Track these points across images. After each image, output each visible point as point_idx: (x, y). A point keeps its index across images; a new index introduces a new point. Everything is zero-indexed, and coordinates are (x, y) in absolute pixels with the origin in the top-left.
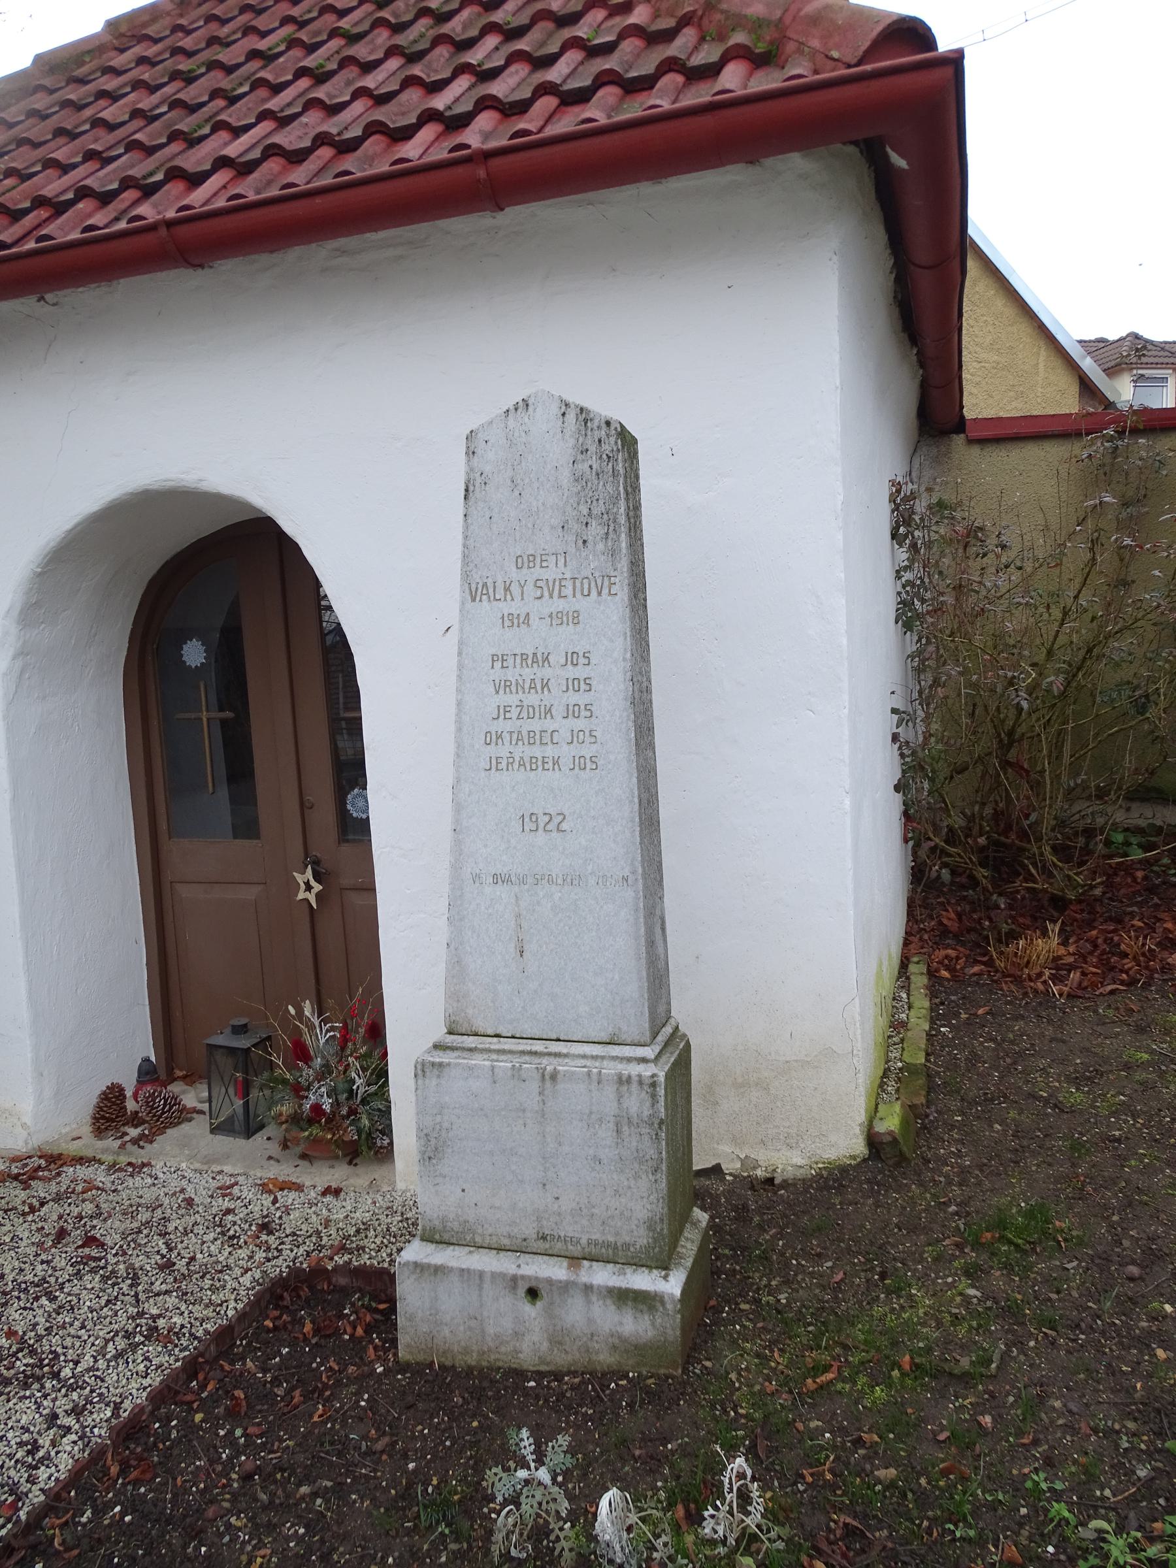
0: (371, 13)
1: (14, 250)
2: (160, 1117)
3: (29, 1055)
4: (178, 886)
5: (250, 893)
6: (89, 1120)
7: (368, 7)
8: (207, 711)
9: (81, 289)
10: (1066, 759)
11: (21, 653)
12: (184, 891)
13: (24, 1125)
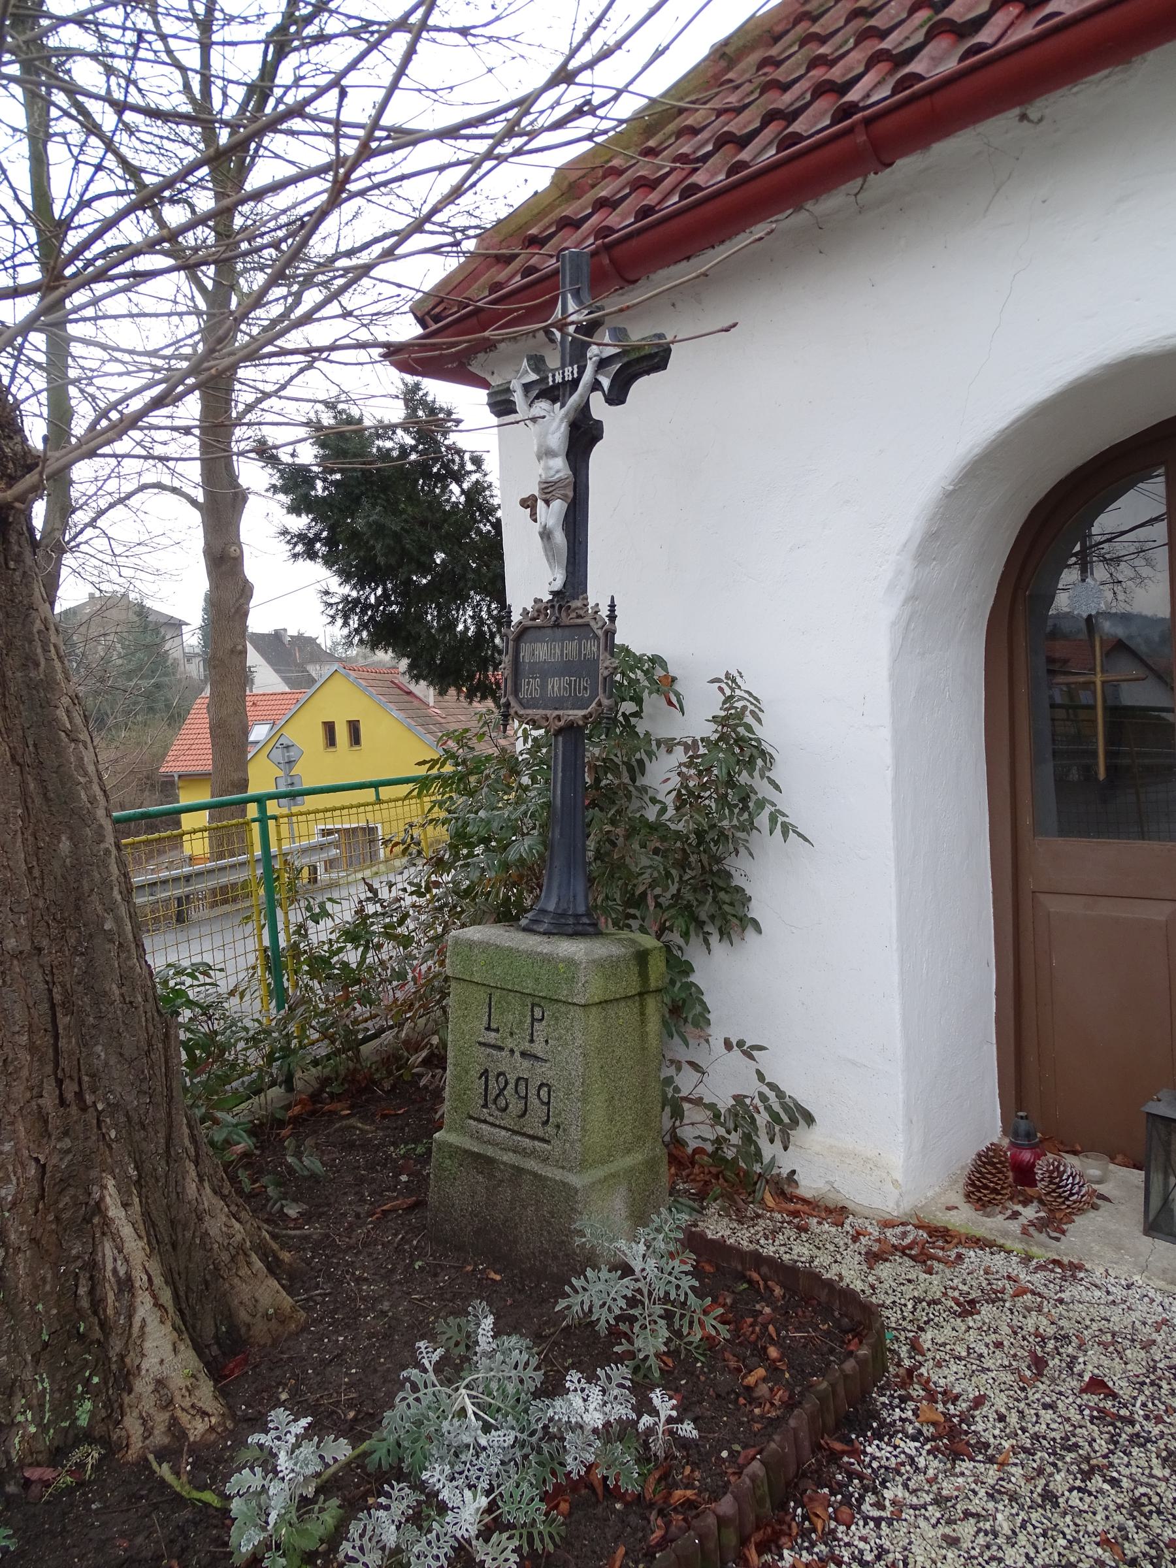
0: (930, 19)
1: (1000, 46)
2: (1067, 1199)
3: (901, 1096)
4: (1042, 897)
5: (1158, 913)
6: (963, 1180)
7: (923, 15)
8: (1103, 671)
9: (1075, 90)
10: (187, 870)
11: (912, 598)
12: (1054, 905)
13: (895, 1182)
